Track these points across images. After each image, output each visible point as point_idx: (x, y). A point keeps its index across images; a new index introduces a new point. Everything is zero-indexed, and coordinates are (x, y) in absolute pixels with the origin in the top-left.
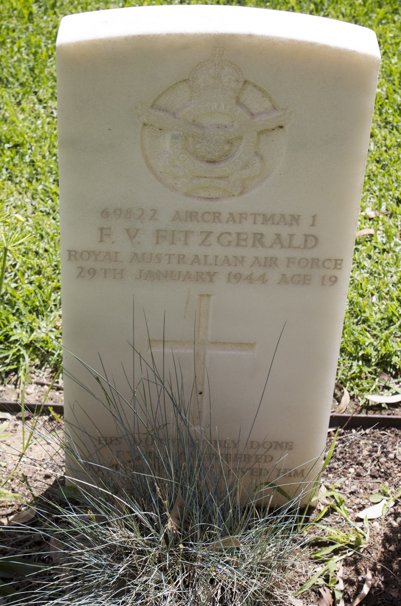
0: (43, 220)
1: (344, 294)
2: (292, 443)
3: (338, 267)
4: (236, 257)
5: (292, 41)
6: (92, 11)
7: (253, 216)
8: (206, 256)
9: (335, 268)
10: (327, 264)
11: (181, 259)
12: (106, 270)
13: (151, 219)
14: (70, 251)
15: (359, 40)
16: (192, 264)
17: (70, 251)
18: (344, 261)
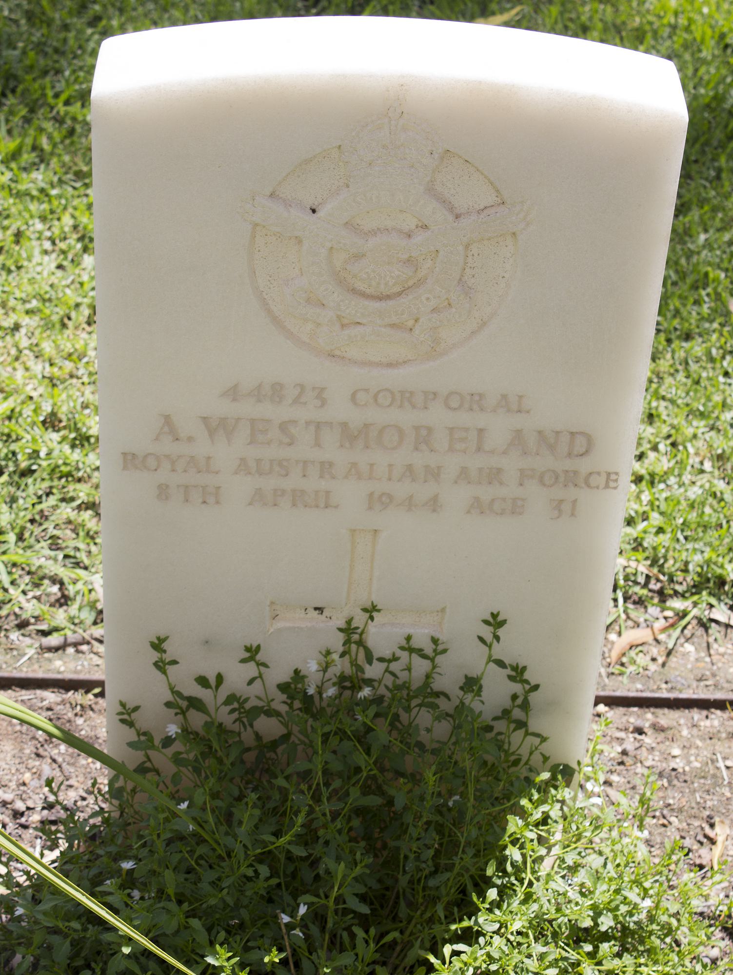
0: (96, 703)
3: (612, 484)
7: (312, 428)
9: (607, 486)
10: (594, 481)
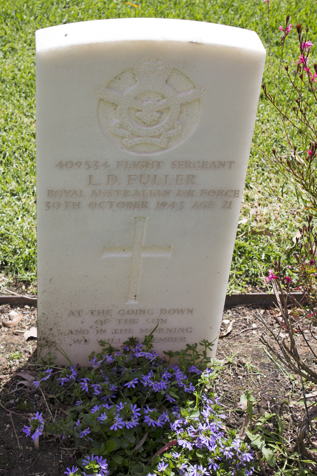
2: (191, 328)
3: (237, 195)
5: (142, 41)
6: (184, 18)
12: (120, 320)
15: (247, 41)
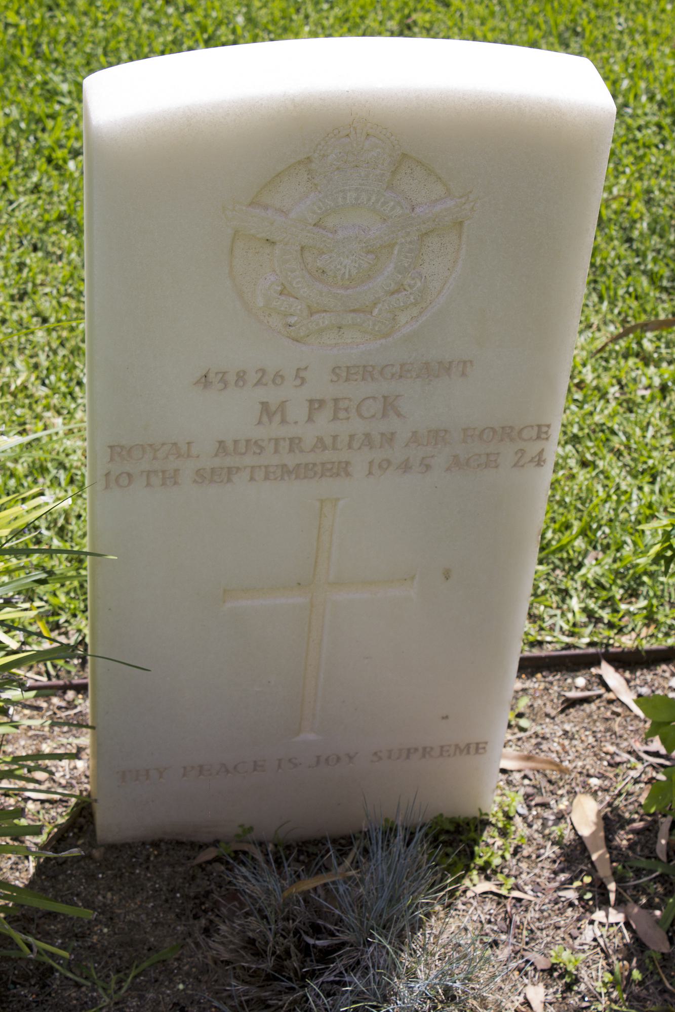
1: (547, 475)
4: (382, 434)
8: (335, 437)
10: (525, 434)
11: (294, 443)
13: (256, 384)
14: (111, 447)
15: (566, 85)
16: (406, 446)
17: (111, 447)
18: (552, 428)
